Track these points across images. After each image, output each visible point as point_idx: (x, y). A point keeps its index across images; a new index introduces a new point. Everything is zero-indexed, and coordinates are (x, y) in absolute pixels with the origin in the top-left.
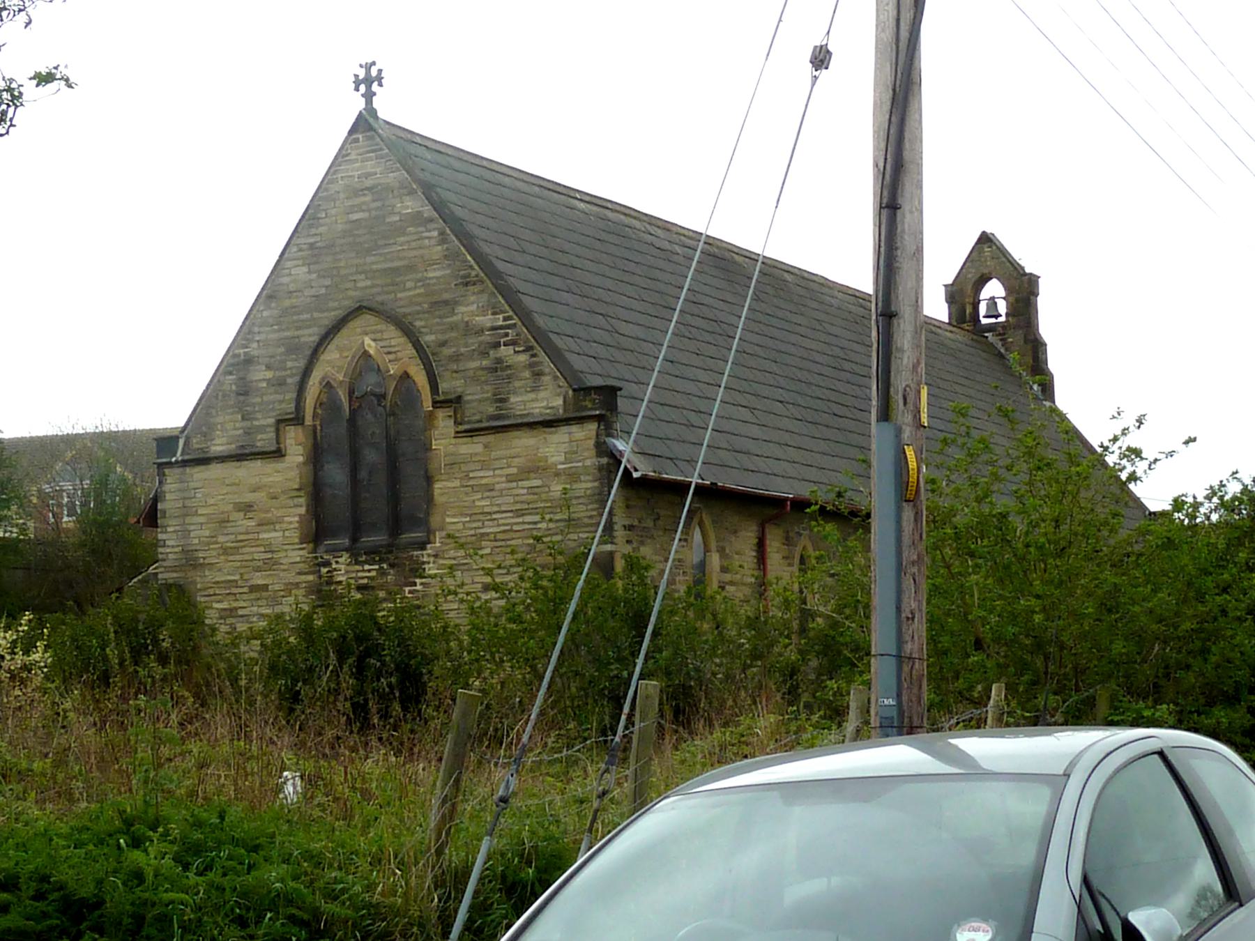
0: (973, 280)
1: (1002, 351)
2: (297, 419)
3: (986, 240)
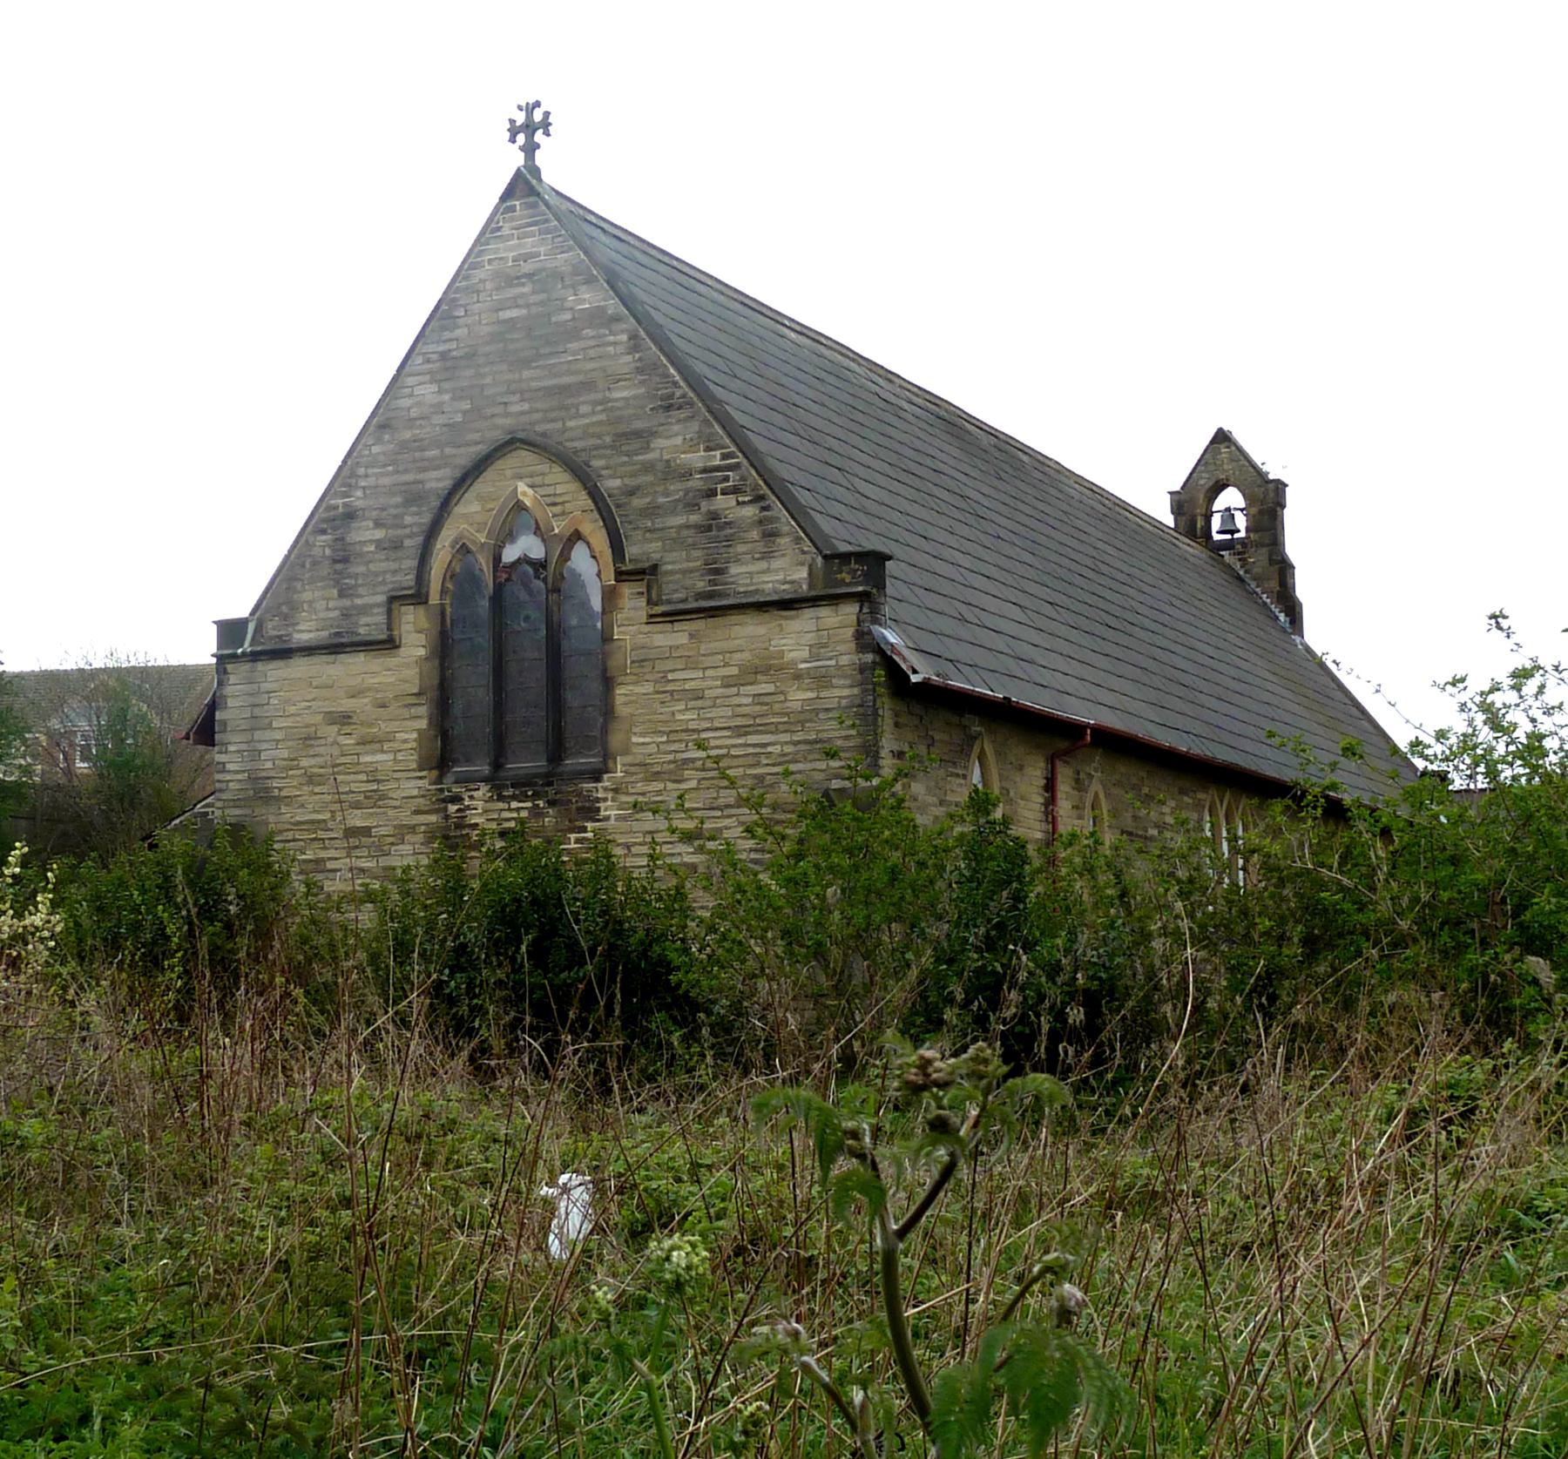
0: (1207, 487)
1: (1241, 573)
3: (1221, 438)
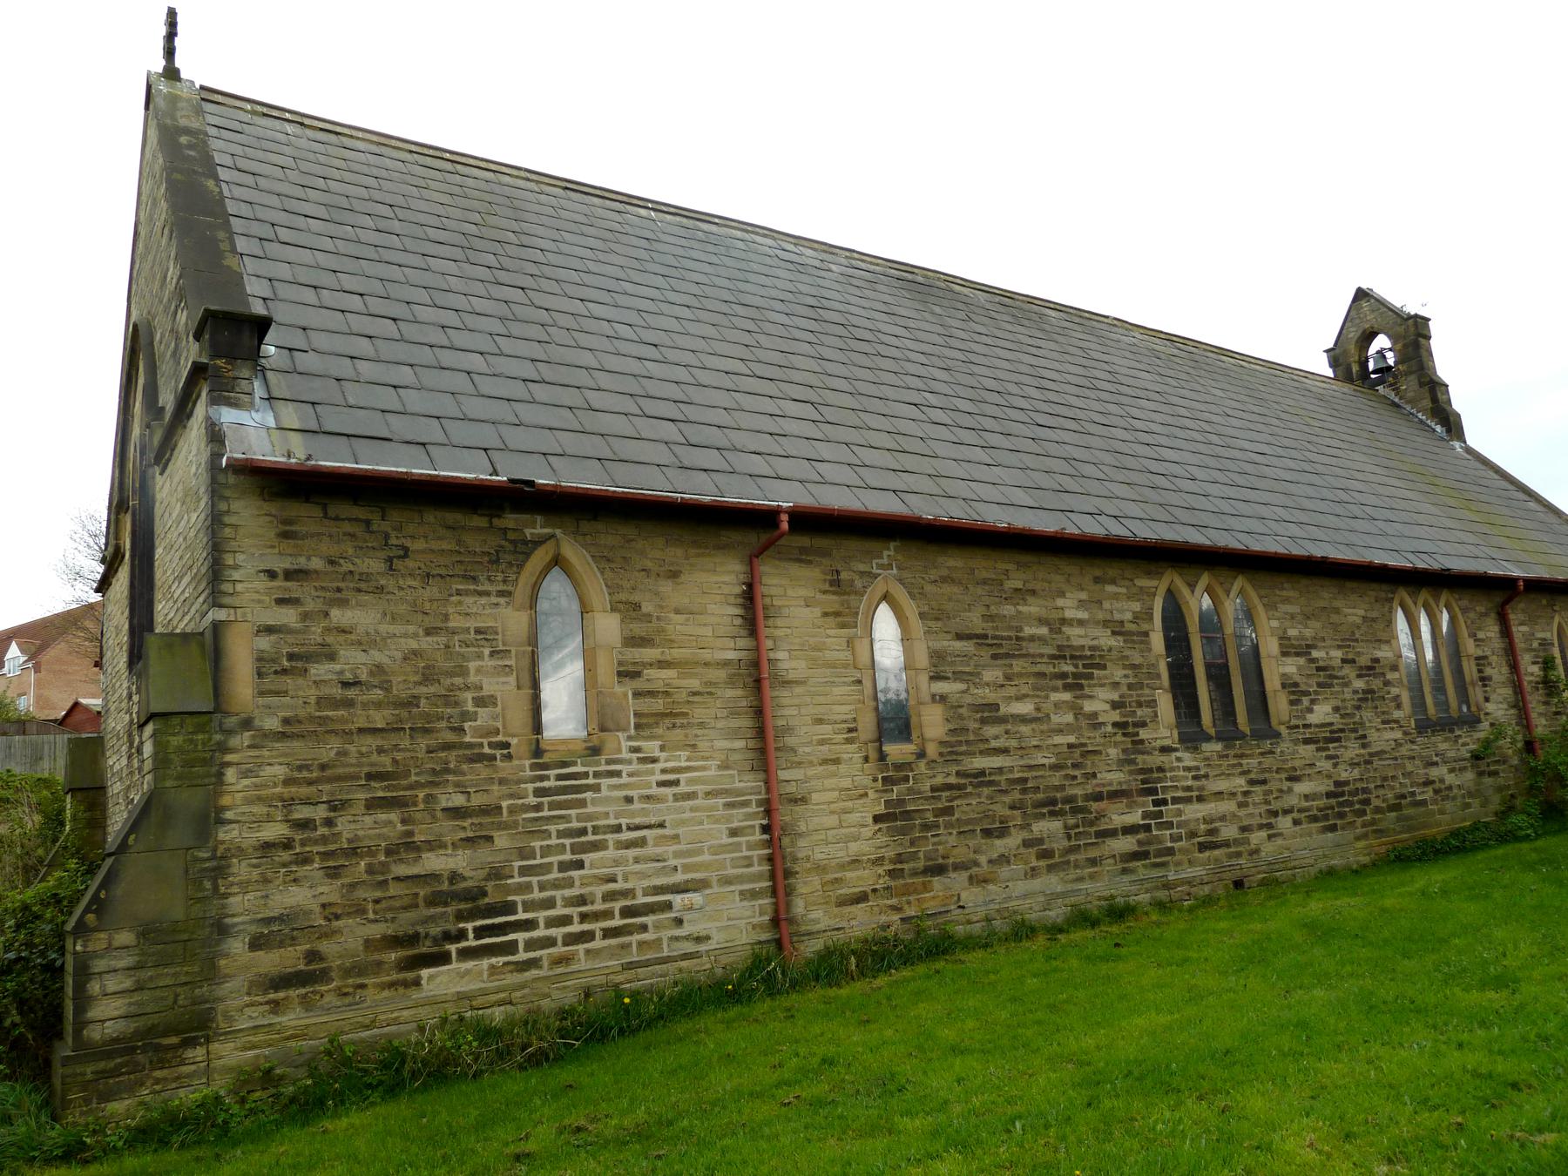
1: (1396, 400)
2: (368, 523)
3: (1361, 295)
